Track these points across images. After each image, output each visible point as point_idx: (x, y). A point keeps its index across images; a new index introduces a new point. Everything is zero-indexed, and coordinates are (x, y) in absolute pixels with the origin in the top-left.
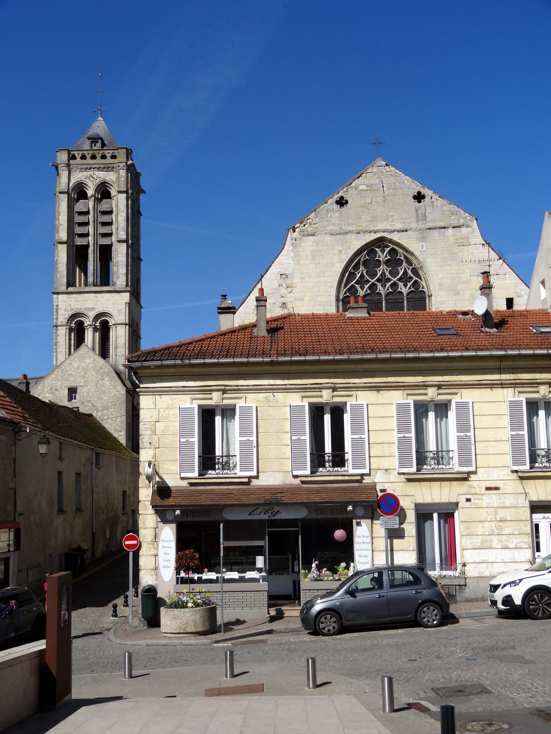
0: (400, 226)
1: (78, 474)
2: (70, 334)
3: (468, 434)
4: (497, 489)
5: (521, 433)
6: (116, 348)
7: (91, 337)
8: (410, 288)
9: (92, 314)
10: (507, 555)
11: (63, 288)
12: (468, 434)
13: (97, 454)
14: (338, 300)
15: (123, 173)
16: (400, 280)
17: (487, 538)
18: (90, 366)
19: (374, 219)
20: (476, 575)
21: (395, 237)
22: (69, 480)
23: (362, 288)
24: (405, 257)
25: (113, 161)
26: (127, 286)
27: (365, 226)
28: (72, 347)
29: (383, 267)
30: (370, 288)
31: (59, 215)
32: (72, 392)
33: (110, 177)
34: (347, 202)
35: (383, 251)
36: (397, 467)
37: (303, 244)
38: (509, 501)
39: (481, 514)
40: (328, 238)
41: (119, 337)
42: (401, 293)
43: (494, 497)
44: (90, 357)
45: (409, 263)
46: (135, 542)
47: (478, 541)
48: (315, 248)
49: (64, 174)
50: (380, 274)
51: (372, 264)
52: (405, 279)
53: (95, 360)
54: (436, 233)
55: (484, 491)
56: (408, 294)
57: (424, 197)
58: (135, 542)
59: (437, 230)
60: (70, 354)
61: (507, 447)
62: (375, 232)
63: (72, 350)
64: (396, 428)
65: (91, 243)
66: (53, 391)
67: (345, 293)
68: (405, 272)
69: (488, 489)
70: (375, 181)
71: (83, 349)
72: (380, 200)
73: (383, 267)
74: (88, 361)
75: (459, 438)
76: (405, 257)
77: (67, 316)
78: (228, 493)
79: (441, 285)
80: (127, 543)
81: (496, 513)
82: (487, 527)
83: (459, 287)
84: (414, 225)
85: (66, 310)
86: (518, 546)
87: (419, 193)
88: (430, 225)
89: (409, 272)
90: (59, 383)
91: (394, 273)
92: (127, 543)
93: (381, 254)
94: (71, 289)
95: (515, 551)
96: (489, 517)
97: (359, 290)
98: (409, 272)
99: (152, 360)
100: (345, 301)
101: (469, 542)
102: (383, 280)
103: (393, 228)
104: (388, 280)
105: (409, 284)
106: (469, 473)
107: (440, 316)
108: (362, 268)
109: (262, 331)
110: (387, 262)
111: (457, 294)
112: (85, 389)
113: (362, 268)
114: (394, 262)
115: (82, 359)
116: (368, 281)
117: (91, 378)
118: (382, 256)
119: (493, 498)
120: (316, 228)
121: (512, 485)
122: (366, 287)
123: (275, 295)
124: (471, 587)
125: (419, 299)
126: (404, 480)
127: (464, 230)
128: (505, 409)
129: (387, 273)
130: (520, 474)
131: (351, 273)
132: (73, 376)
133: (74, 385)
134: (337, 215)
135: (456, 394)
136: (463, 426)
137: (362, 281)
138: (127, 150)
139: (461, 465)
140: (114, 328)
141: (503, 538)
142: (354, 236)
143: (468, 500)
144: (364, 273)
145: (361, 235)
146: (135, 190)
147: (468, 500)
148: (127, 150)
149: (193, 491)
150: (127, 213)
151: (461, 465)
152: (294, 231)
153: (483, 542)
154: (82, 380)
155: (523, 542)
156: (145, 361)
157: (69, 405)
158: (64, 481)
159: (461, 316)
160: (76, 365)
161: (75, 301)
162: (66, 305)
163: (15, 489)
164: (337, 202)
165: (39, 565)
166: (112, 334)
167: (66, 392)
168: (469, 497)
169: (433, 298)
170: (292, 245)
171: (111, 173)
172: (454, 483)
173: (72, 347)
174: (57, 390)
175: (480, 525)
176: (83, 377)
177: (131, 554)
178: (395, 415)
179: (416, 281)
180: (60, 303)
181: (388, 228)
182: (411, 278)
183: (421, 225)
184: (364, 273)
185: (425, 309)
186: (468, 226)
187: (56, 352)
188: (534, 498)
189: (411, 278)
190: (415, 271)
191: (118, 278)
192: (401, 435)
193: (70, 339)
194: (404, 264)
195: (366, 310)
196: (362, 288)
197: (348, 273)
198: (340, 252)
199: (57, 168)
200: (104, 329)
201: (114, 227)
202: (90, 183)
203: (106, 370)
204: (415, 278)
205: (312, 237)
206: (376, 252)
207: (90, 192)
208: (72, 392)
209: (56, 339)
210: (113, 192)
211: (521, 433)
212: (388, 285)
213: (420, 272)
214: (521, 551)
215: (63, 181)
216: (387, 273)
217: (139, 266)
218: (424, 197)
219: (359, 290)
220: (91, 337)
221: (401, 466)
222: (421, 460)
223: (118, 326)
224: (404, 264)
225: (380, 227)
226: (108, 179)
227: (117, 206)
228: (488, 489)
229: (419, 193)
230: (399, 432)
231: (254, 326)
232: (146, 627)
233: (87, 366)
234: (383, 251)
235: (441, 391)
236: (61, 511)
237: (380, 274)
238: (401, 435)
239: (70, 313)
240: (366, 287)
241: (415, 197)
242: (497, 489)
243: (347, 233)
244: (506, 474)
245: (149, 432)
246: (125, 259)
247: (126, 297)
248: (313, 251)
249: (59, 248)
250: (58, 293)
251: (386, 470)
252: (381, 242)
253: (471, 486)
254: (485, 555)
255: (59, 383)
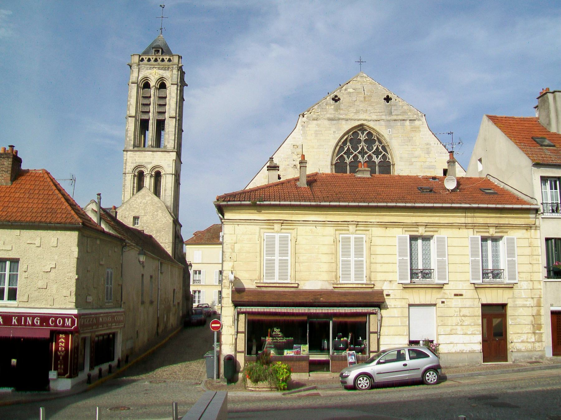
0: (374, 117)
1: (151, 277)
2: (134, 179)
3: (444, 259)
4: (461, 295)
5: (477, 259)
6: (165, 190)
7: (148, 182)
8: (380, 159)
9: (150, 167)
10: (466, 339)
11: (131, 148)
12: (444, 259)
13: (161, 263)
14: (332, 165)
15: (175, 71)
16: (359, 153)
17: (454, 327)
18: (149, 202)
19: (357, 112)
20: (446, 352)
21: (371, 124)
22: (147, 279)
23: (348, 157)
24: (378, 138)
25: (169, 63)
26: (174, 148)
27: (351, 116)
28: (135, 189)
29: (363, 143)
30: (353, 157)
31: (131, 98)
32: (136, 218)
33: (166, 74)
34: (339, 99)
35: (363, 133)
36: (398, 279)
37: (309, 126)
38: (468, 303)
39: (451, 312)
40: (327, 123)
41: (167, 182)
42: (374, 162)
43: (459, 300)
44: (149, 196)
45: (380, 142)
46: (218, 325)
47: (448, 329)
48: (318, 129)
49: (135, 69)
50: (361, 150)
51: (355, 142)
52: (377, 153)
53: (152, 198)
54: (399, 123)
55: (453, 296)
56: (350, 163)
57: (391, 99)
58: (218, 325)
59: (399, 121)
60: (133, 194)
61: (469, 268)
62: (358, 120)
63: (135, 191)
64: (397, 253)
65: (151, 118)
66: (123, 218)
67: (337, 160)
68: (377, 148)
69: (456, 295)
70: (359, 86)
71: (143, 191)
72: (362, 99)
73: (363, 143)
74: (147, 198)
75: (438, 261)
76: (378, 138)
77: (133, 167)
78: (284, 293)
79: (401, 158)
80: (213, 325)
81: (460, 311)
82: (455, 320)
83: (413, 160)
84: (384, 117)
85: (132, 163)
86: (474, 332)
87: (388, 96)
88: (395, 117)
89: (380, 148)
90: (127, 213)
91: (356, 149)
92: (213, 325)
93: (361, 135)
94: (136, 149)
95: (471, 336)
96: (456, 313)
97: (346, 158)
98: (380, 148)
99: (234, 201)
100: (339, 166)
101: (442, 330)
102: (363, 153)
103: (370, 118)
104: (366, 153)
105: (380, 156)
106: (444, 284)
107: (394, 177)
108: (348, 144)
109: (303, 183)
110: (366, 141)
111: (412, 164)
112: (145, 218)
113: (348, 144)
114: (370, 140)
115: (144, 197)
116: (352, 153)
117: (149, 210)
118: (363, 137)
119: (458, 301)
120: (319, 115)
121: (469, 293)
122: (351, 156)
123: (289, 159)
124: (443, 360)
125: (386, 166)
126: (402, 288)
127: (417, 123)
128: (467, 242)
129: (365, 148)
130: (476, 286)
131: (341, 147)
132: (136, 208)
133: (137, 215)
134: (332, 107)
135: (437, 231)
136: (441, 253)
137: (348, 153)
138: (179, 57)
139: (439, 279)
140: (164, 177)
141: (464, 327)
142: (344, 122)
143: (443, 302)
144: (350, 147)
145: (349, 122)
146: (182, 84)
147: (443, 302)
148: (179, 57)
149: (259, 292)
150: (177, 99)
151: (439, 279)
152: (303, 116)
153: (451, 330)
154: (143, 212)
155: (477, 330)
156: (229, 201)
157: (134, 227)
158: (144, 281)
159: (431, 180)
160: (139, 201)
161: (138, 157)
162: (133, 159)
163: (122, 285)
164: (333, 99)
165: (132, 338)
166: (163, 181)
167: (132, 219)
168: (443, 300)
169: (395, 166)
170: (302, 126)
171: (167, 72)
172: (435, 290)
173: (135, 189)
174: (125, 217)
175: (450, 318)
176: (144, 209)
177: (216, 333)
178: (397, 245)
179: (384, 154)
180: (128, 158)
181: (367, 118)
182: (381, 152)
183: (389, 118)
184: (350, 147)
185: (389, 172)
186: (419, 120)
187: (124, 191)
188: (485, 302)
189: (381, 152)
190: (384, 148)
191: (168, 142)
192: (401, 258)
193: (134, 183)
194: (377, 143)
195: (369, 173)
196: (348, 157)
197: (340, 147)
198: (334, 132)
199: (131, 66)
200: (158, 176)
201: (167, 107)
202: (152, 78)
203: (160, 205)
204: (384, 153)
205: (315, 122)
206: (358, 134)
207: (152, 83)
208: (136, 218)
209: (125, 182)
210: (168, 84)
211: (477, 259)
212: (366, 156)
213: (387, 148)
214: (475, 336)
215: (134, 76)
216: (365, 148)
217: (181, 134)
218: (391, 99)
219: (346, 158)
220: (148, 182)
221: (400, 279)
222: (413, 274)
223: (167, 175)
224: (377, 143)
225: (362, 116)
226: (165, 76)
227: (170, 94)
228: (456, 295)
229: (388, 96)
230: (400, 256)
231: (297, 180)
232: (226, 383)
233: (147, 202)
234: (363, 133)
235: (427, 229)
236: (143, 303)
237: (361, 150)
238: (401, 258)
239: (135, 165)
240: (351, 156)
241: (385, 99)
242: (461, 295)
243: (347, 120)
244: (467, 285)
245: (230, 250)
246: (174, 130)
247: (173, 155)
248: (316, 131)
249: (129, 121)
250: (127, 151)
251: (390, 281)
252: (361, 128)
253: (445, 293)
254: (453, 339)
255: (127, 213)
